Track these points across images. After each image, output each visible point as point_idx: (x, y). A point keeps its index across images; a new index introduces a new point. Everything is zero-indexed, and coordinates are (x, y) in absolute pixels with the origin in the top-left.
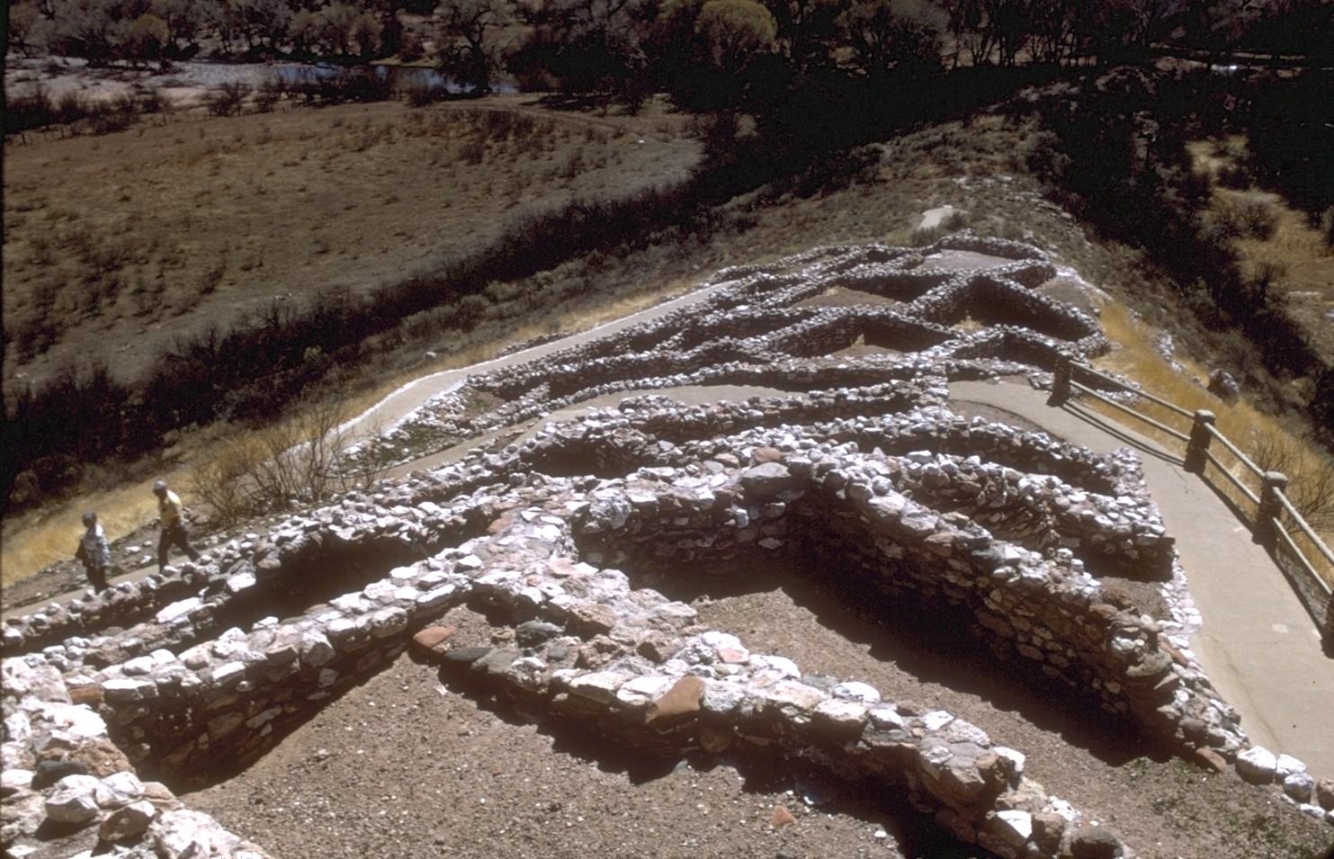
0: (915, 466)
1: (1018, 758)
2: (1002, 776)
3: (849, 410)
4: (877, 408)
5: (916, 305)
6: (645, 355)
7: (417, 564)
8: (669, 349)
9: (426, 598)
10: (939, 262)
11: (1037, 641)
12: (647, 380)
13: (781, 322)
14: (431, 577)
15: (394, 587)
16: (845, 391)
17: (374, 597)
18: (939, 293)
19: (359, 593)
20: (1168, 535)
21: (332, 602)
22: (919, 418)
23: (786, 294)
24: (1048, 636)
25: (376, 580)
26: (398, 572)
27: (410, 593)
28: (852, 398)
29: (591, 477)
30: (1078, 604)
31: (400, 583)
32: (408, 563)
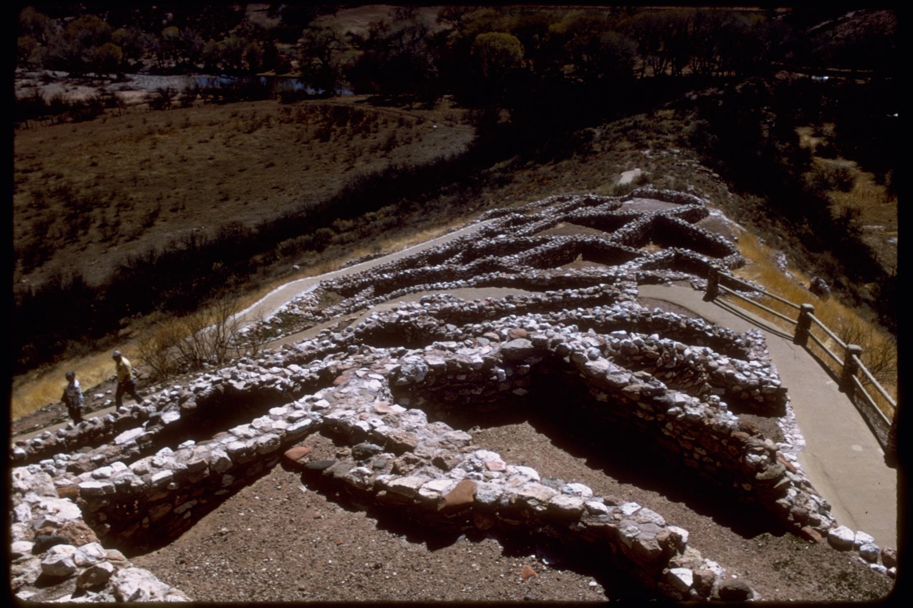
0: (616, 341)
1: (684, 533)
2: (672, 546)
3: (572, 304)
4: (591, 303)
5: (616, 234)
6: (438, 267)
7: (287, 405)
8: (454, 264)
9: (293, 428)
10: (632, 206)
11: (696, 456)
12: (439, 284)
13: (527, 246)
14: (296, 414)
15: (272, 421)
16: (569, 291)
17: (258, 427)
18: (631, 227)
19: (248, 425)
20: (783, 386)
21: (231, 430)
22: (617, 310)
23: (530, 227)
24: (704, 453)
25: (260, 416)
26: (274, 411)
27: (282, 424)
28: (574, 296)
29: (402, 348)
30: (724, 432)
31: (275, 418)
32: (281, 405)
